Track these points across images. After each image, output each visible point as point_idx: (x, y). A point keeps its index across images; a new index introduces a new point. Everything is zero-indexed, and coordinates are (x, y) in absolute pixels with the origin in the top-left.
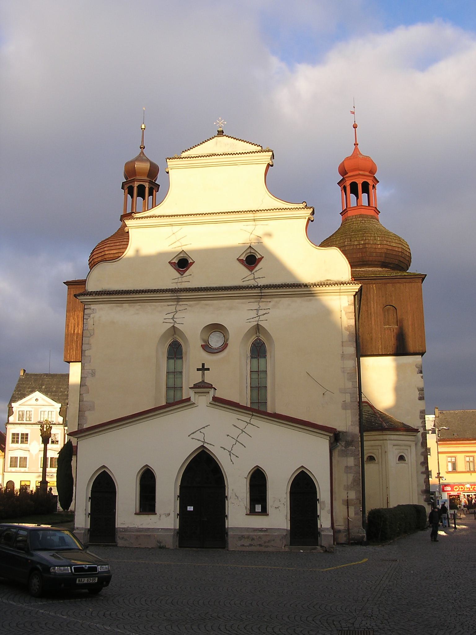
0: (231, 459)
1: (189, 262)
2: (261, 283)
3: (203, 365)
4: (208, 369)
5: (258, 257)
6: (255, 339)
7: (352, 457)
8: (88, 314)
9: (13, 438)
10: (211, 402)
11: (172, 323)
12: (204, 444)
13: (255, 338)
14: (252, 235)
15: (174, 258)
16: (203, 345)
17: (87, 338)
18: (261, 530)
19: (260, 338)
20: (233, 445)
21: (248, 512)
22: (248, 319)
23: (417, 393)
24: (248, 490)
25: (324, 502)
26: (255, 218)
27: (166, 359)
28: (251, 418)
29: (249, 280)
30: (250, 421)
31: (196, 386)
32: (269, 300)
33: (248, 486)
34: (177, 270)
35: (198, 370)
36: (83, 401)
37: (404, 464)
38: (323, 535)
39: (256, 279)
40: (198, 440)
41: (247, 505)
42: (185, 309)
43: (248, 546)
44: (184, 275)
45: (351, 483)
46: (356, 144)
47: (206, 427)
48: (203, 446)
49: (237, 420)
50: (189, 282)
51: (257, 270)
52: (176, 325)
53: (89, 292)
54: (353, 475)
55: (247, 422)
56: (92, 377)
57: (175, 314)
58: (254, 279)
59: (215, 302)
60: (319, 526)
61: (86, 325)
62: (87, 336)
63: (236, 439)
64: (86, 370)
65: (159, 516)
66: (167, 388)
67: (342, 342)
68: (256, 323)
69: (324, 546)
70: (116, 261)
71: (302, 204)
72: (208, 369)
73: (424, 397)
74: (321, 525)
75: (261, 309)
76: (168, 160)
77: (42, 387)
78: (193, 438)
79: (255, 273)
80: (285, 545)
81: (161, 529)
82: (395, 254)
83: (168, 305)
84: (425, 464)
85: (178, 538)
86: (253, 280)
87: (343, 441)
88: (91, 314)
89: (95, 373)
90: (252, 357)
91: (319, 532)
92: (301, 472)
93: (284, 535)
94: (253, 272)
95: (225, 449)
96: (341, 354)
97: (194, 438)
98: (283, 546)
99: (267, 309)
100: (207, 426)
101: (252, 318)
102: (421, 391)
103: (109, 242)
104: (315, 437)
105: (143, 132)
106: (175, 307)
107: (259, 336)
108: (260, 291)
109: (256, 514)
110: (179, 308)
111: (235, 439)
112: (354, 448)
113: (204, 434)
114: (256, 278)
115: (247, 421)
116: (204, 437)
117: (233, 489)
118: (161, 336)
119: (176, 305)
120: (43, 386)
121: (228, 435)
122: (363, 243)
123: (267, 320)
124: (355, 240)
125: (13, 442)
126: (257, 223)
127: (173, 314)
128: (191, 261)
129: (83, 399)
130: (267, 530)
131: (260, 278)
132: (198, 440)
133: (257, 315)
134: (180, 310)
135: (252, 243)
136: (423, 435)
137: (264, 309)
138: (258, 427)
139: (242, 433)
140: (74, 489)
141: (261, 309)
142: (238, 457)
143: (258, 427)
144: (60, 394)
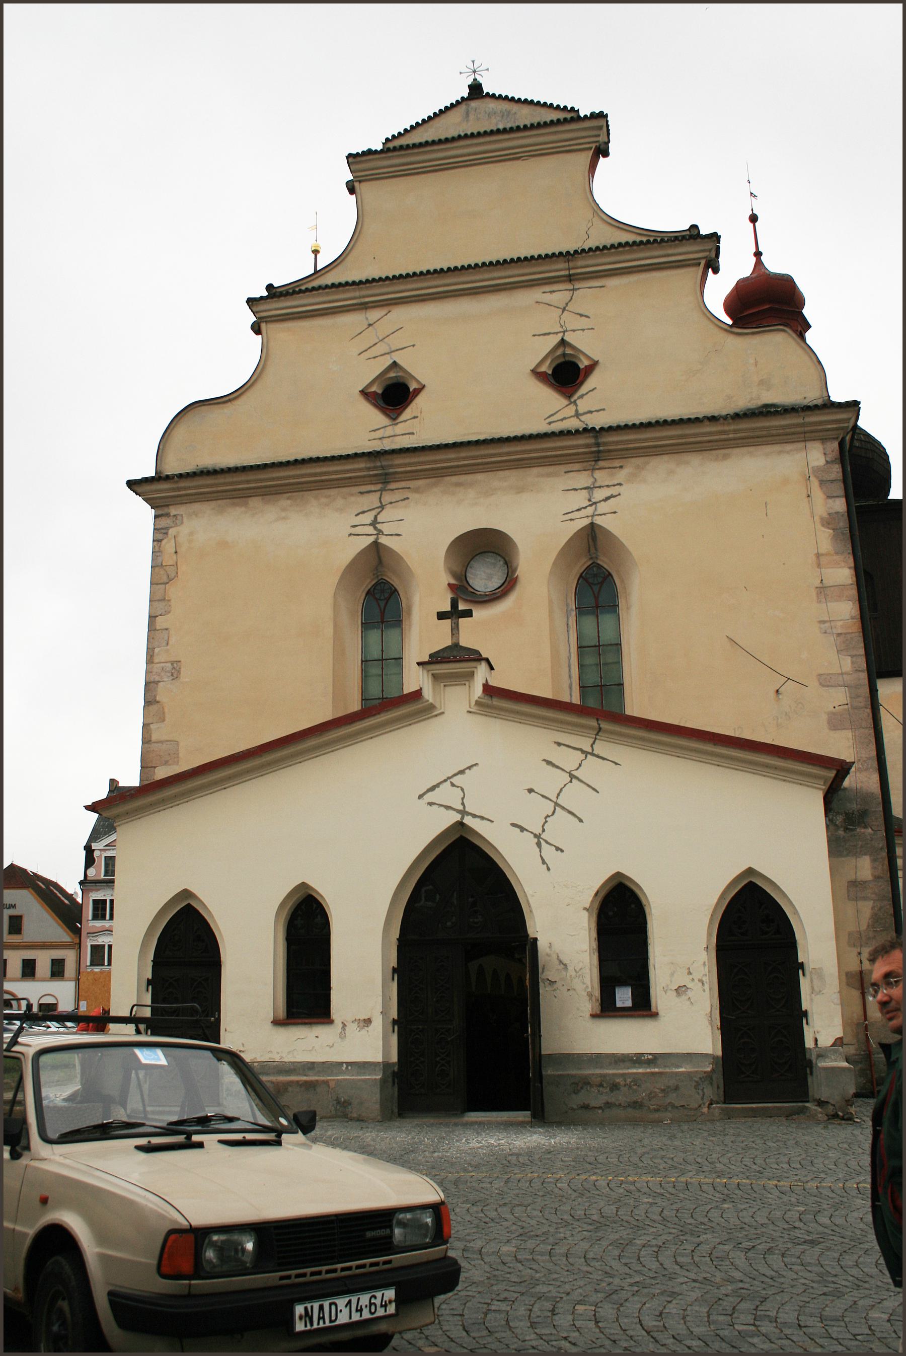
0: (541, 855)
1: (411, 390)
7: (865, 854)
8: (162, 529)
9: (95, 909)
11: (371, 535)
12: (463, 818)
13: (585, 563)
14: (565, 312)
16: (453, 584)
18: (637, 1059)
20: (546, 818)
22: (567, 513)
24: (595, 945)
25: (819, 972)
26: (572, 272)
27: (360, 628)
28: (596, 739)
29: (565, 418)
30: (592, 746)
31: (436, 658)
33: (594, 934)
35: (441, 616)
38: (826, 1069)
40: (448, 808)
41: (592, 987)
42: (404, 499)
43: (600, 1108)
45: (868, 926)
46: (758, 254)
48: (461, 824)
49: (556, 746)
50: (413, 434)
52: (383, 540)
54: (871, 903)
55: (583, 751)
56: (173, 680)
58: (577, 415)
63: (555, 800)
64: (159, 665)
65: (341, 1025)
66: (362, 700)
67: (818, 555)
68: (586, 522)
69: (827, 1102)
74: (816, 1040)
78: (431, 804)
79: (578, 402)
80: (711, 1100)
81: (346, 1063)
85: (396, 1089)
87: (838, 813)
88: (171, 527)
89: (179, 672)
91: (810, 1061)
92: (746, 886)
93: (705, 1072)
94: (572, 400)
95: (522, 829)
96: (817, 588)
97: (434, 804)
98: (707, 1104)
99: (614, 485)
100: (469, 768)
101: (578, 510)
110: (387, 497)
111: (551, 800)
112: (870, 830)
113: (462, 790)
114: (581, 411)
115: (585, 749)
116: (463, 799)
118: (344, 568)
119: (382, 490)
121: (531, 791)
123: (615, 512)
125: (95, 917)
127: (374, 513)
129: (151, 736)
130: (655, 1059)
131: (591, 412)
132: (448, 808)
133: (590, 500)
134: (391, 503)
135: (567, 331)
137: (608, 486)
138: (616, 764)
139: (571, 782)
141: (600, 487)
142: (562, 851)
143: (616, 764)
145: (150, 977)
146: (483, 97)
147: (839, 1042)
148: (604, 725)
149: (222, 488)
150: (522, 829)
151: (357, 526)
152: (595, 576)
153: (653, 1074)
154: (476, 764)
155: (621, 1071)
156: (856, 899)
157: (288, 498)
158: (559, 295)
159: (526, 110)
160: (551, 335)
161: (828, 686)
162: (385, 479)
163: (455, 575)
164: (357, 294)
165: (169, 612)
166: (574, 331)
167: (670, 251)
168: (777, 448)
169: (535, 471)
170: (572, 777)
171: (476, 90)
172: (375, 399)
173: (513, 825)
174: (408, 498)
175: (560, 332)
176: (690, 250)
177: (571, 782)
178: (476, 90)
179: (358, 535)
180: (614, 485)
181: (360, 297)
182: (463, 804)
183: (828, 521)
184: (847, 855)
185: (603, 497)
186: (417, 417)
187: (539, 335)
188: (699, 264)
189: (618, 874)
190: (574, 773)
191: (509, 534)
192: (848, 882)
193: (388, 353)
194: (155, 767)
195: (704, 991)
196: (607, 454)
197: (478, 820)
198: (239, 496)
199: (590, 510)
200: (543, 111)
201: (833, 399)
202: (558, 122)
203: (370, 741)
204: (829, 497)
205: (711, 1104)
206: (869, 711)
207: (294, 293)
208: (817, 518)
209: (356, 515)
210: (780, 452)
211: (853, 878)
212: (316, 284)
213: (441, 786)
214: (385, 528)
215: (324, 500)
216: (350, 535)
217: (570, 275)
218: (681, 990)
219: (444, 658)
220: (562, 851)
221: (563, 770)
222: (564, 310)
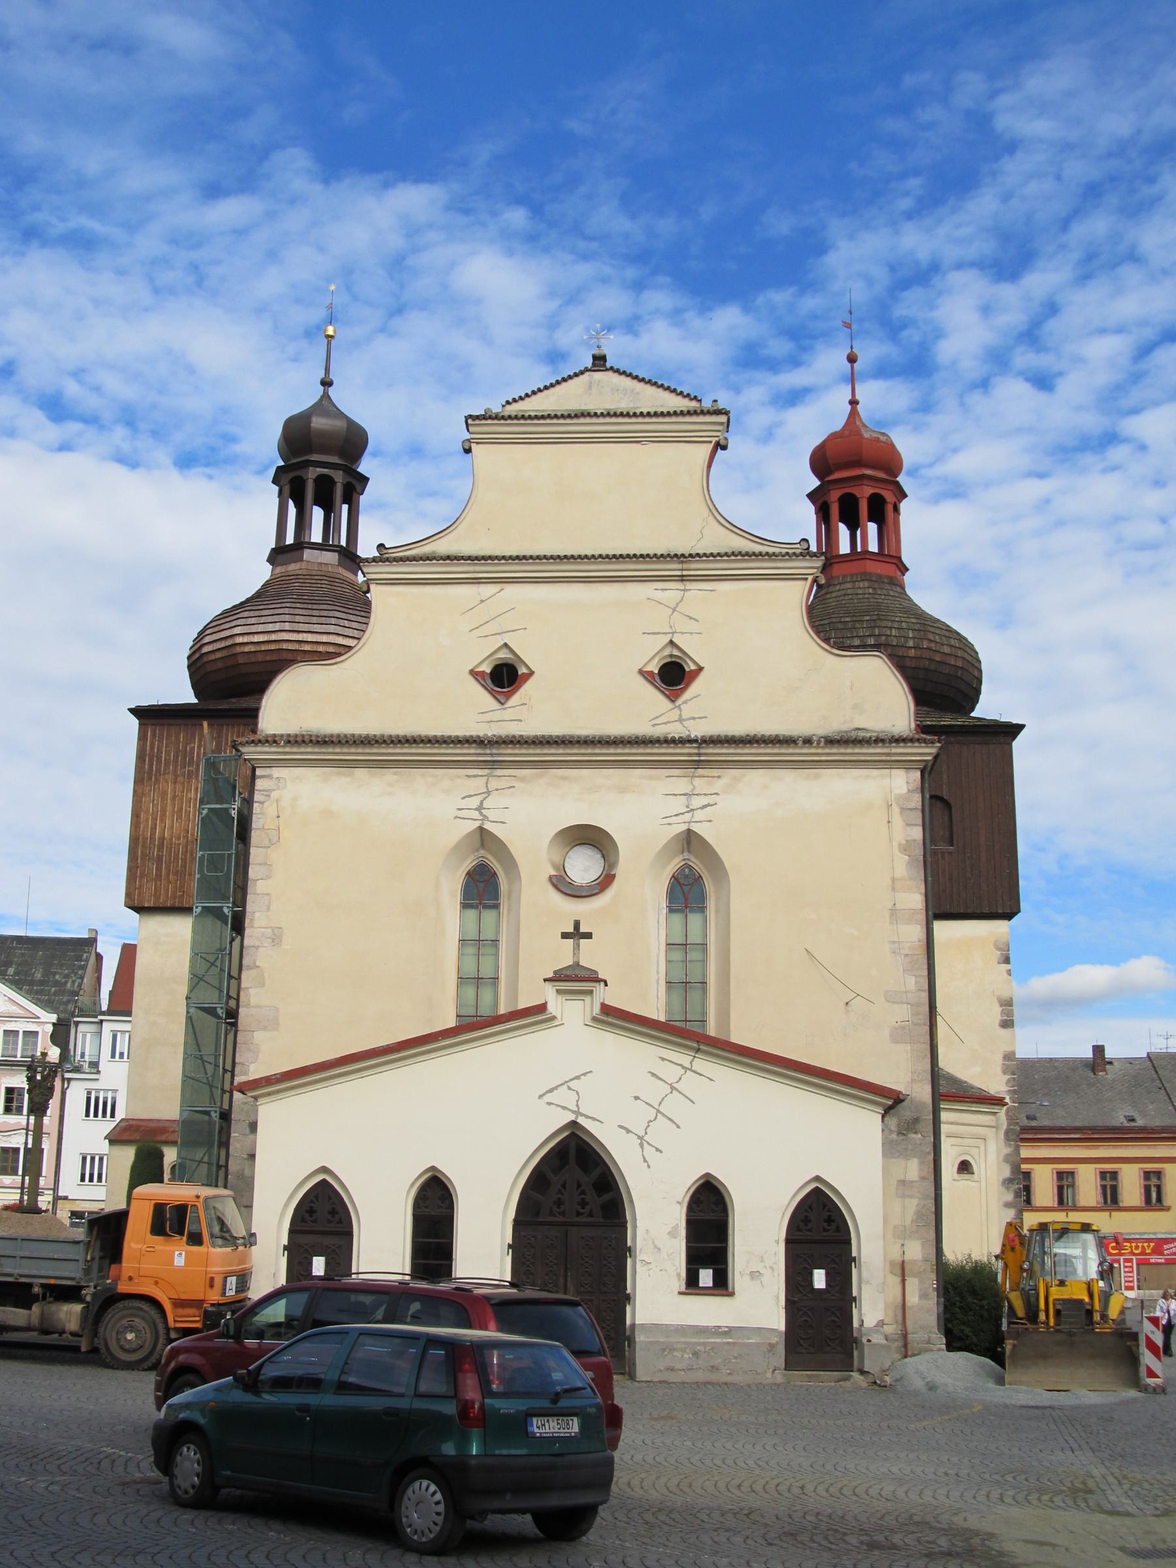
2: (698, 730)
3: (577, 925)
4: (588, 936)
5: (689, 666)
6: (679, 866)
7: (914, 1157)
11: (477, 820)
12: (577, 1118)
18: (716, 1331)
19: (691, 864)
20: (648, 1123)
21: (683, 1288)
23: (997, 1009)
26: (685, 573)
29: (669, 722)
31: (558, 977)
32: (716, 772)
34: (490, 692)
35: (565, 936)
37: (970, 1182)
39: (685, 720)
40: (564, 1108)
44: (507, 705)
45: (912, 1221)
48: (574, 1123)
49: (660, 1060)
50: (521, 721)
51: (689, 698)
52: (488, 826)
53: (267, 736)
54: (915, 1201)
55: (683, 1067)
57: (484, 799)
58: (681, 720)
59: (585, 772)
60: (856, 1324)
61: (260, 816)
63: (657, 1107)
67: (893, 880)
68: (684, 827)
70: (336, 663)
71: (798, 546)
72: (588, 936)
73: (1013, 1020)
75: (697, 795)
76: (470, 421)
77: (7, 970)
78: (549, 1104)
79: (682, 706)
82: (947, 671)
83: (467, 776)
84: (1013, 1184)
86: (678, 724)
88: (274, 790)
90: (671, 910)
94: (677, 705)
95: (628, 1131)
98: (771, 1370)
99: (711, 794)
100: (584, 1074)
101: (676, 815)
102: (1005, 1005)
103: (246, 614)
104: (849, 1106)
105: (329, 344)
106: (485, 781)
108: (696, 751)
109: (702, 1292)
110: (494, 784)
111: (654, 1107)
112: (920, 1135)
113: (577, 1093)
116: (577, 1101)
120: (11, 967)
121: (637, 1098)
122: (872, 643)
123: (710, 821)
124: (855, 634)
126: (689, 585)
127: (480, 798)
129: (249, 1001)
130: (730, 1331)
131: (694, 718)
132: (564, 1108)
133: (687, 807)
134: (497, 790)
135: (675, 632)
136: (1010, 1114)
137: (705, 795)
138: (711, 1080)
139: (671, 1093)
141: (697, 795)
142: (661, 1152)
143: (711, 1080)
144: (53, 989)
145: (286, 1244)
146: (607, 370)
147: (881, 1323)
148: (702, 1047)
152: (686, 877)
153: (728, 1343)
154: (591, 1072)
155: (702, 1340)
156: (903, 1196)
157: (395, 774)
161: (893, 1002)
163: (555, 867)
164: (471, 568)
165: (271, 877)
166: (683, 633)
170: (673, 1088)
172: (484, 679)
173: (620, 1127)
174: (514, 787)
175: (669, 633)
179: (464, 819)
180: (711, 794)
182: (577, 1106)
183: (905, 848)
184: (899, 1157)
186: (526, 704)
187: (649, 634)
188: (806, 579)
189: (708, 1175)
190: (675, 1085)
192: (898, 1181)
193: (499, 634)
195: (774, 1276)
199: (687, 817)
200: (667, 395)
204: (908, 825)
205: (775, 1370)
206: (927, 1028)
208: (895, 844)
209: (462, 798)
211: (902, 1177)
215: (430, 780)
216: (456, 817)
218: (755, 1275)
219: (567, 976)
220: (661, 1152)
222: (674, 610)
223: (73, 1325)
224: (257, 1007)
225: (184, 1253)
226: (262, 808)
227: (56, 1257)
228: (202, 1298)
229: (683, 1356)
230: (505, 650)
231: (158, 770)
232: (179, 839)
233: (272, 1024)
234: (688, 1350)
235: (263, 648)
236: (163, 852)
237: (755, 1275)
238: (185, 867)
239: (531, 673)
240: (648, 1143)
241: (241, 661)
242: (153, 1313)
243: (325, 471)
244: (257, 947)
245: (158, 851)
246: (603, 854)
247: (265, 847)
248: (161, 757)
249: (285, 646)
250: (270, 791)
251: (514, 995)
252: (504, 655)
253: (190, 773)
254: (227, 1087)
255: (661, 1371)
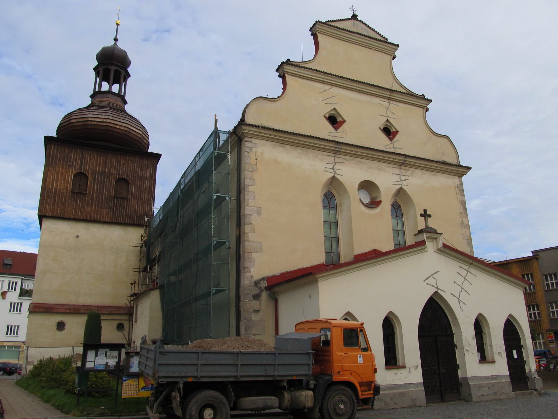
10: (441, 247)
11: (332, 173)
12: (437, 290)
15: (327, 113)
17: (249, 172)
18: (488, 378)
19: (397, 201)
26: (391, 97)
30: (469, 269)
36: (249, 241)
43: (486, 395)
47: (437, 273)
49: (459, 268)
52: (337, 176)
56: (258, 215)
60: (527, 371)
62: (250, 170)
64: (251, 207)
78: (428, 284)
79: (394, 143)
86: (393, 149)
88: (253, 148)
95: (454, 296)
101: (397, 182)
107: (396, 199)
108: (404, 159)
110: (337, 160)
113: (436, 280)
116: (437, 283)
117: (466, 337)
123: (407, 185)
128: (341, 120)
129: (249, 239)
133: (400, 179)
134: (338, 162)
138: (476, 276)
139: (465, 280)
140: (25, 331)
141: (403, 175)
143: (476, 276)
149: (278, 138)
150: (454, 296)
151: (327, 168)
157: (301, 150)
158: (385, 103)
159: (372, 32)
160: (384, 117)
162: (337, 152)
164: (323, 77)
167: (419, 101)
168: (448, 176)
169: (384, 164)
171: (354, 17)
173: (451, 294)
176: (421, 102)
177: (465, 280)
178: (354, 17)
181: (324, 79)
182: (437, 285)
185: (404, 179)
186: (344, 132)
191: (377, 184)
193: (332, 104)
194: (251, 253)
196: (405, 164)
197: (441, 291)
198: (283, 142)
199: (400, 183)
201: (461, 164)
202: (380, 41)
203: (407, 258)
207: (297, 66)
210: (449, 177)
212: (306, 66)
213: (430, 278)
214: (337, 171)
217: (389, 98)
220: (465, 304)
221: (462, 276)
223: (310, 403)
224: (252, 242)
225: (362, 356)
226: (249, 155)
227: (298, 362)
228: (372, 380)
229: (485, 389)
230: (334, 111)
231: (56, 163)
232: (63, 190)
233: (259, 250)
234: (486, 387)
235: (100, 124)
236: (56, 194)
237: (500, 353)
238: (66, 202)
239: (344, 121)
240: (461, 301)
241: (90, 127)
242: (350, 391)
243: (118, 69)
244: (251, 215)
245: (54, 194)
246: (369, 193)
247: (251, 171)
248: (57, 157)
249: (109, 125)
250: (252, 148)
251: (351, 245)
252: (333, 112)
253: (69, 166)
254: (136, 286)
255: (480, 396)
